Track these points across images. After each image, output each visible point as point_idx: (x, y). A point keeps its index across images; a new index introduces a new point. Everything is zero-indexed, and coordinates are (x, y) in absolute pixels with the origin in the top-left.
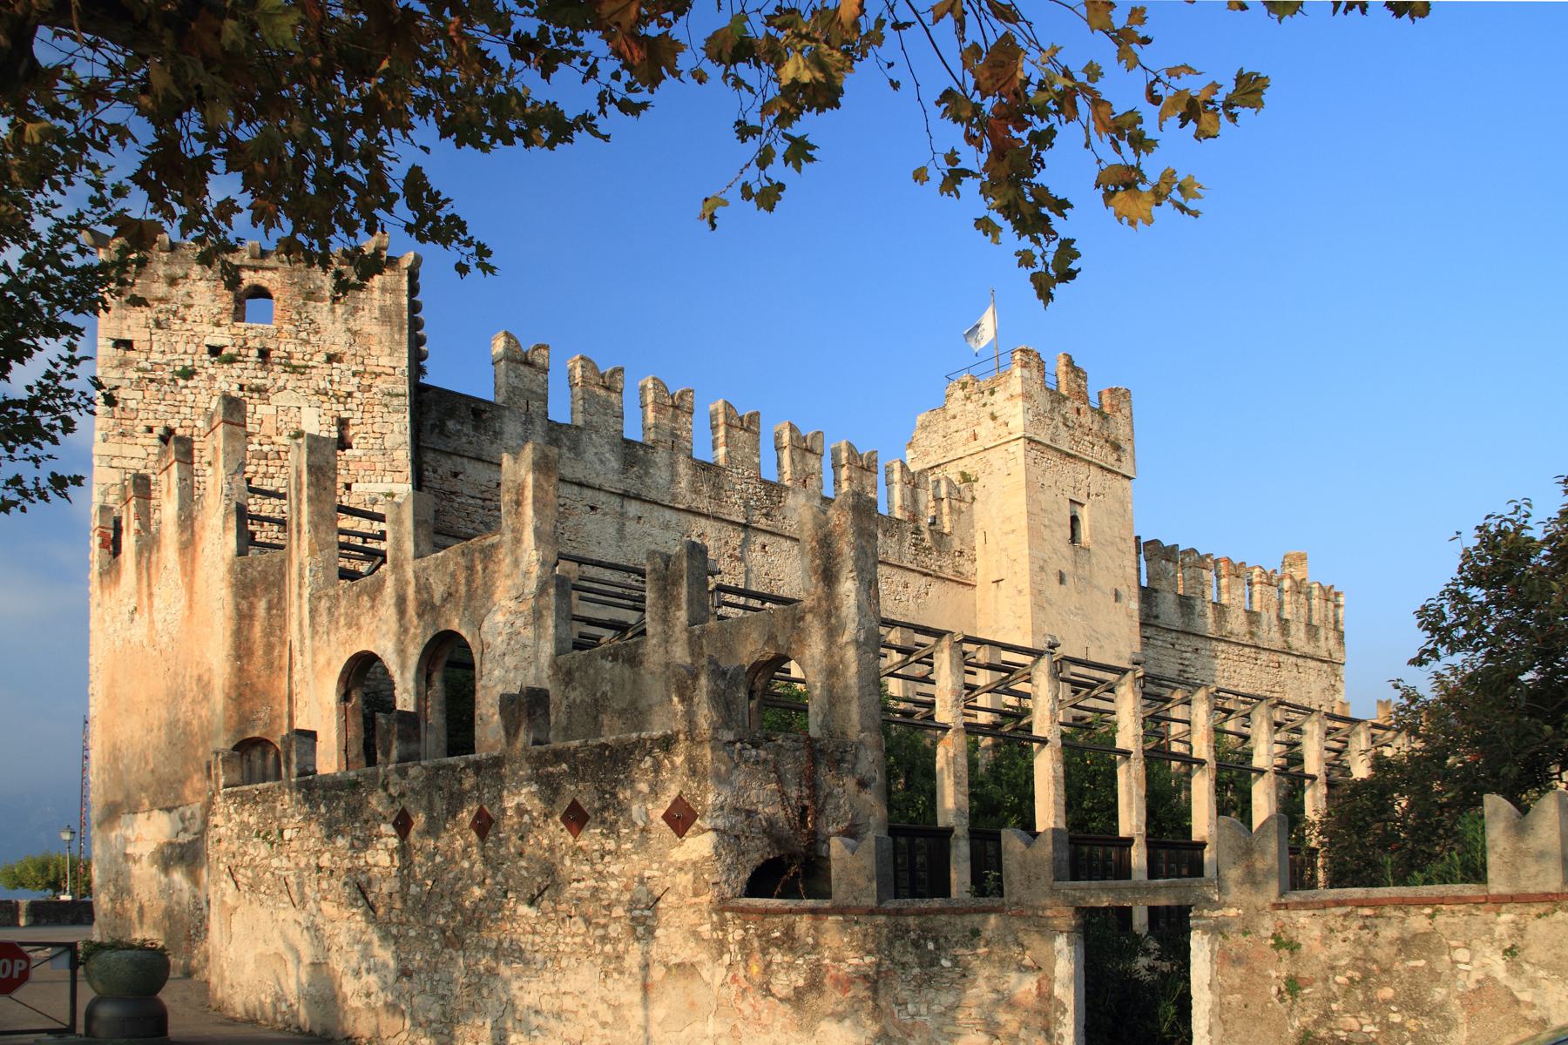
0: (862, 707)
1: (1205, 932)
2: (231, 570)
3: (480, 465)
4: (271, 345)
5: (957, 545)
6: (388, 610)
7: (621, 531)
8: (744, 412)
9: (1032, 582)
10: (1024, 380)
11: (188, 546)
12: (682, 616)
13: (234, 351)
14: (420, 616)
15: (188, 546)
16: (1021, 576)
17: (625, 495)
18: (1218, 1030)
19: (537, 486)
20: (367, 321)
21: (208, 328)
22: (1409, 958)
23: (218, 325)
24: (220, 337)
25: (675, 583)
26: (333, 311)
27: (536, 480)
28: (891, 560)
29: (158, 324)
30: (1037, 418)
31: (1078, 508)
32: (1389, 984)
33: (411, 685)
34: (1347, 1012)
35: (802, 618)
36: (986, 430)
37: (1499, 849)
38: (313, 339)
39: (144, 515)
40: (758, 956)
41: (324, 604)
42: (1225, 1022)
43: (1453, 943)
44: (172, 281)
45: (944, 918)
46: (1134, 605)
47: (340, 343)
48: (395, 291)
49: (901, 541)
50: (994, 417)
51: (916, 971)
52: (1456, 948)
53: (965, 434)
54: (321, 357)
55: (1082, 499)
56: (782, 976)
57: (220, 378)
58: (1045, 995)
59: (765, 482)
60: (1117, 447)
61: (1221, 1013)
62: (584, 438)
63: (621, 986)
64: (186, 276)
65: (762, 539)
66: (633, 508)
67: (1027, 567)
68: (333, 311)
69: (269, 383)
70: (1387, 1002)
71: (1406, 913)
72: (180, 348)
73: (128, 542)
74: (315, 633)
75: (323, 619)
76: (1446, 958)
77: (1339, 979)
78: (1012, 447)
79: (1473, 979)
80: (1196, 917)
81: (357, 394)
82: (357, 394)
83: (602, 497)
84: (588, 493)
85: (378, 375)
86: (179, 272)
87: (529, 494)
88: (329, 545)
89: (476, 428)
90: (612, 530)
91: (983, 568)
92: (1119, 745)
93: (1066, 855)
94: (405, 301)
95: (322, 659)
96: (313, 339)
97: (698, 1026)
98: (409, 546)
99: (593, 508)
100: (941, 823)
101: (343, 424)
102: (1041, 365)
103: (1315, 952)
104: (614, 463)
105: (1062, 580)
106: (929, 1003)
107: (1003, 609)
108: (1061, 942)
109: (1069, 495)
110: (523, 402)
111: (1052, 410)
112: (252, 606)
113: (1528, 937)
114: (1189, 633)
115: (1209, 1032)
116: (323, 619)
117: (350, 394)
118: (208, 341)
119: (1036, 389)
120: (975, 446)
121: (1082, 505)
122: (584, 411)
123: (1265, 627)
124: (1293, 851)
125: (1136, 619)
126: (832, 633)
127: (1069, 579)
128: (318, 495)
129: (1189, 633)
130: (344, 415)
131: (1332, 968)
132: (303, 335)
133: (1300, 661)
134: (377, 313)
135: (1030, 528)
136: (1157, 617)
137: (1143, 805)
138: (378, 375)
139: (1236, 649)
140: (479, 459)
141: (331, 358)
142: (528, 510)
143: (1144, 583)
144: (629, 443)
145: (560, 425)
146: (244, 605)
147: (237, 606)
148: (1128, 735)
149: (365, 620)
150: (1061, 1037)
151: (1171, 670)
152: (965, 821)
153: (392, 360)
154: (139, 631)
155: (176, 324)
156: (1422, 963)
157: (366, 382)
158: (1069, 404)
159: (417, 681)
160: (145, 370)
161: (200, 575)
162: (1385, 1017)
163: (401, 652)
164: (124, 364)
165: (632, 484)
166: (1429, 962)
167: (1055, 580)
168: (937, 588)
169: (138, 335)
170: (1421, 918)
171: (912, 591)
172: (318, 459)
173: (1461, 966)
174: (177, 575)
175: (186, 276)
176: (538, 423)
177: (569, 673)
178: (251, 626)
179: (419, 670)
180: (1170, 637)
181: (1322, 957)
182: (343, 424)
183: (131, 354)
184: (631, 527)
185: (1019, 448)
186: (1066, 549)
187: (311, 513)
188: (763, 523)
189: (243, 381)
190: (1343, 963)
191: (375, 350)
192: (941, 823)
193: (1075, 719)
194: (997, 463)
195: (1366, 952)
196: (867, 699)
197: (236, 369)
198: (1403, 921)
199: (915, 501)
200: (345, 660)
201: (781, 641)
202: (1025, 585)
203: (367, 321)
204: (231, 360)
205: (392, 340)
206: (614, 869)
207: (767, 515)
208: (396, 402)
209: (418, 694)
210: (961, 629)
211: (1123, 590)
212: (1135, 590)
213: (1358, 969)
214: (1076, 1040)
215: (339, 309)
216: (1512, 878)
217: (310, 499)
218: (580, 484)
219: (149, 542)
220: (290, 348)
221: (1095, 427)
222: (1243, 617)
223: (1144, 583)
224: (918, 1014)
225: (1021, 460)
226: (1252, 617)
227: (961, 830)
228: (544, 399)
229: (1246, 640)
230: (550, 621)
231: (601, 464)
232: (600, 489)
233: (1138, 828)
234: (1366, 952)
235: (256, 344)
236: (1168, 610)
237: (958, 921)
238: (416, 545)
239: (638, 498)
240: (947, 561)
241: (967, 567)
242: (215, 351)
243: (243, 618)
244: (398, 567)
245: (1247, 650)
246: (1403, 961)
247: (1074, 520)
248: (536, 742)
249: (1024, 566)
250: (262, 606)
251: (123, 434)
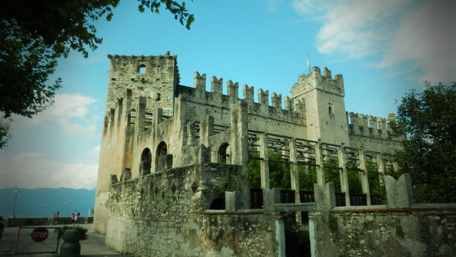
0: (243, 156)
1: (312, 220)
2: (126, 130)
3: (190, 103)
4: (145, 77)
5: (301, 116)
6: (151, 137)
7: (222, 117)
8: (250, 87)
9: (320, 124)
10: (316, 74)
11: (119, 125)
12: (207, 134)
13: (136, 79)
14: (157, 138)
15: (119, 125)
16: (317, 123)
17: (223, 108)
18: (318, 253)
19: (181, 105)
20: (165, 71)
21: (132, 75)
22: (368, 230)
23: (134, 74)
24: (134, 77)
25: (206, 126)
26: (158, 69)
27: (181, 103)
28: (286, 121)
29: (121, 75)
30: (319, 84)
31: (331, 106)
32: (363, 239)
33: (155, 155)
34: (352, 248)
35: (230, 133)
36: (307, 87)
37: (390, 193)
38: (154, 76)
39: (113, 119)
40: (209, 227)
41: (140, 137)
42: (319, 250)
43: (380, 225)
44: (125, 65)
45: (250, 215)
46: (347, 129)
47: (159, 76)
48: (171, 64)
49: (288, 116)
50: (309, 84)
51: (244, 231)
52: (381, 227)
53: (303, 88)
54: (155, 80)
55: (331, 102)
56: (214, 233)
57: (134, 86)
58: (274, 240)
59: (255, 103)
60: (339, 89)
61: (318, 247)
62: (214, 95)
63: (180, 237)
64: (128, 63)
65: (255, 117)
66: (225, 111)
67: (318, 120)
68: (158, 69)
69: (144, 86)
70: (363, 245)
71: (366, 214)
72: (125, 79)
73: (109, 125)
74: (138, 144)
75: (140, 140)
76: (378, 230)
77: (349, 236)
78: (313, 91)
79: (386, 238)
80: (310, 215)
81: (162, 88)
82: (162, 88)
83: (218, 109)
84: (214, 108)
85: (167, 83)
86: (126, 62)
87: (179, 107)
88: (143, 122)
89: (189, 94)
90: (220, 117)
91: (308, 122)
92: (340, 166)
93: (279, 196)
94: (173, 66)
95: (138, 150)
96: (154, 76)
97: (195, 249)
98: (156, 121)
99: (216, 112)
100: (292, 189)
101: (159, 95)
102: (320, 70)
103: (342, 227)
104: (220, 100)
105: (327, 123)
106: (247, 242)
107: (313, 133)
108: (277, 222)
109: (328, 102)
110: (200, 88)
111: (323, 81)
112: (129, 138)
113: (401, 223)
114: (363, 136)
115: (315, 253)
116: (140, 140)
117: (161, 88)
118: (131, 77)
119: (319, 76)
120: (305, 91)
121: (332, 104)
122: (214, 89)
123: (383, 133)
124: (337, 194)
125: (347, 133)
126: (237, 136)
127: (329, 123)
128: (141, 110)
129: (363, 136)
130: (159, 92)
131: (347, 233)
132: (152, 75)
133: (395, 143)
134: (167, 69)
135: (319, 111)
136: (354, 132)
137: (347, 183)
138: (167, 83)
139: (376, 140)
140: (190, 101)
141: (157, 80)
142: (179, 111)
143: (350, 123)
144: (224, 96)
145: (208, 92)
146: (128, 138)
147: (126, 139)
148: (342, 163)
149: (147, 140)
150: (278, 254)
151: (359, 146)
152: (298, 189)
153: (170, 79)
154: (109, 146)
155: (125, 74)
156: (371, 231)
157: (164, 85)
158: (327, 79)
159: (156, 154)
160: (118, 85)
161: (120, 131)
162: (363, 250)
163: (154, 147)
164: (114, 84)
165: (225, 106)
166: (373, 231)
167: (325, 123)
168: (297, 127)
169: (117, 77)
170: (370, 216)
171: (291, 128)
172: (142, 102)
173: (383, 233)
174: (116, 132)
175: (128, 63)
176: (203, 92)
177: (185, 151)
178: (129, 144)
179: (157, 152)
180: (358, 137)
181: (344, 229)
182: (159, 95)
183: (115, 82)
184: (224, 116)
185: (315, 91)
186: (328, 116)
187: (139, 115)
188: (255, 113)
189: (139, 86)
190: (350, 231)
191: (167, 77)
192: (342, 192)
193: (331, 160)
194: (310, 95)
195: (356, 228)
196: (244, 154)
197: (137, 84)
198: (365, 217)
199: (291, 106)
200: (143, 150)
201: (226, 139)
202: (318, 125)
203: (165, 71)
204: (136, 82)
205: (170, 75)
206: (181, 202)
207: (255, 111)
208: (171, 89)
209: (156, 157)
210: (295, 137)
211: (343, 125)
212: (347, 125)
213: (354, 233)
214: (284, 254)
215: (160, 69)
216: (395, 203)
217: (139, 111)
218: (213, 106)
219: (112, 125)
220: (149, 78)
221: (334, 84)
222: (377, 131)
223: (350, 123)
224: (244, 245)
225: (316, 94)
226: (380, 131)
227: (297, 191)
228: (205, 86)
229: (378, 137)
230: (182, 137)
231: (217, 101)
232: (217, 107)
233: (347, 190)
234: (356, 228)
235: (141, 77)
236: (357, 131)
237: (253, 216)
238: (158, 121)
239: (226, 108)
240: (299, 120)
241: (304, 122)
242: (133, 80)
243: (127, 141)
244: (154, 126)
245: (379, 140)
246: (366, 231)
247: (330, 108)
248: (169, 168)
249: (318, 121)
250: (131, 138)
251: (112, 100)
